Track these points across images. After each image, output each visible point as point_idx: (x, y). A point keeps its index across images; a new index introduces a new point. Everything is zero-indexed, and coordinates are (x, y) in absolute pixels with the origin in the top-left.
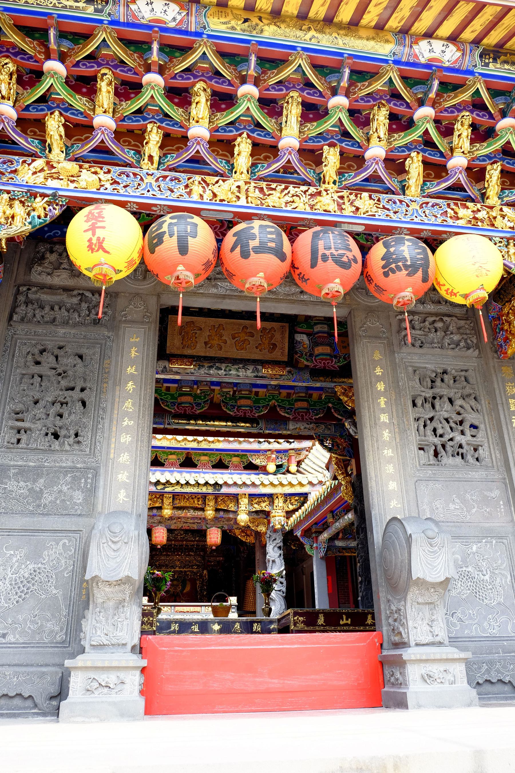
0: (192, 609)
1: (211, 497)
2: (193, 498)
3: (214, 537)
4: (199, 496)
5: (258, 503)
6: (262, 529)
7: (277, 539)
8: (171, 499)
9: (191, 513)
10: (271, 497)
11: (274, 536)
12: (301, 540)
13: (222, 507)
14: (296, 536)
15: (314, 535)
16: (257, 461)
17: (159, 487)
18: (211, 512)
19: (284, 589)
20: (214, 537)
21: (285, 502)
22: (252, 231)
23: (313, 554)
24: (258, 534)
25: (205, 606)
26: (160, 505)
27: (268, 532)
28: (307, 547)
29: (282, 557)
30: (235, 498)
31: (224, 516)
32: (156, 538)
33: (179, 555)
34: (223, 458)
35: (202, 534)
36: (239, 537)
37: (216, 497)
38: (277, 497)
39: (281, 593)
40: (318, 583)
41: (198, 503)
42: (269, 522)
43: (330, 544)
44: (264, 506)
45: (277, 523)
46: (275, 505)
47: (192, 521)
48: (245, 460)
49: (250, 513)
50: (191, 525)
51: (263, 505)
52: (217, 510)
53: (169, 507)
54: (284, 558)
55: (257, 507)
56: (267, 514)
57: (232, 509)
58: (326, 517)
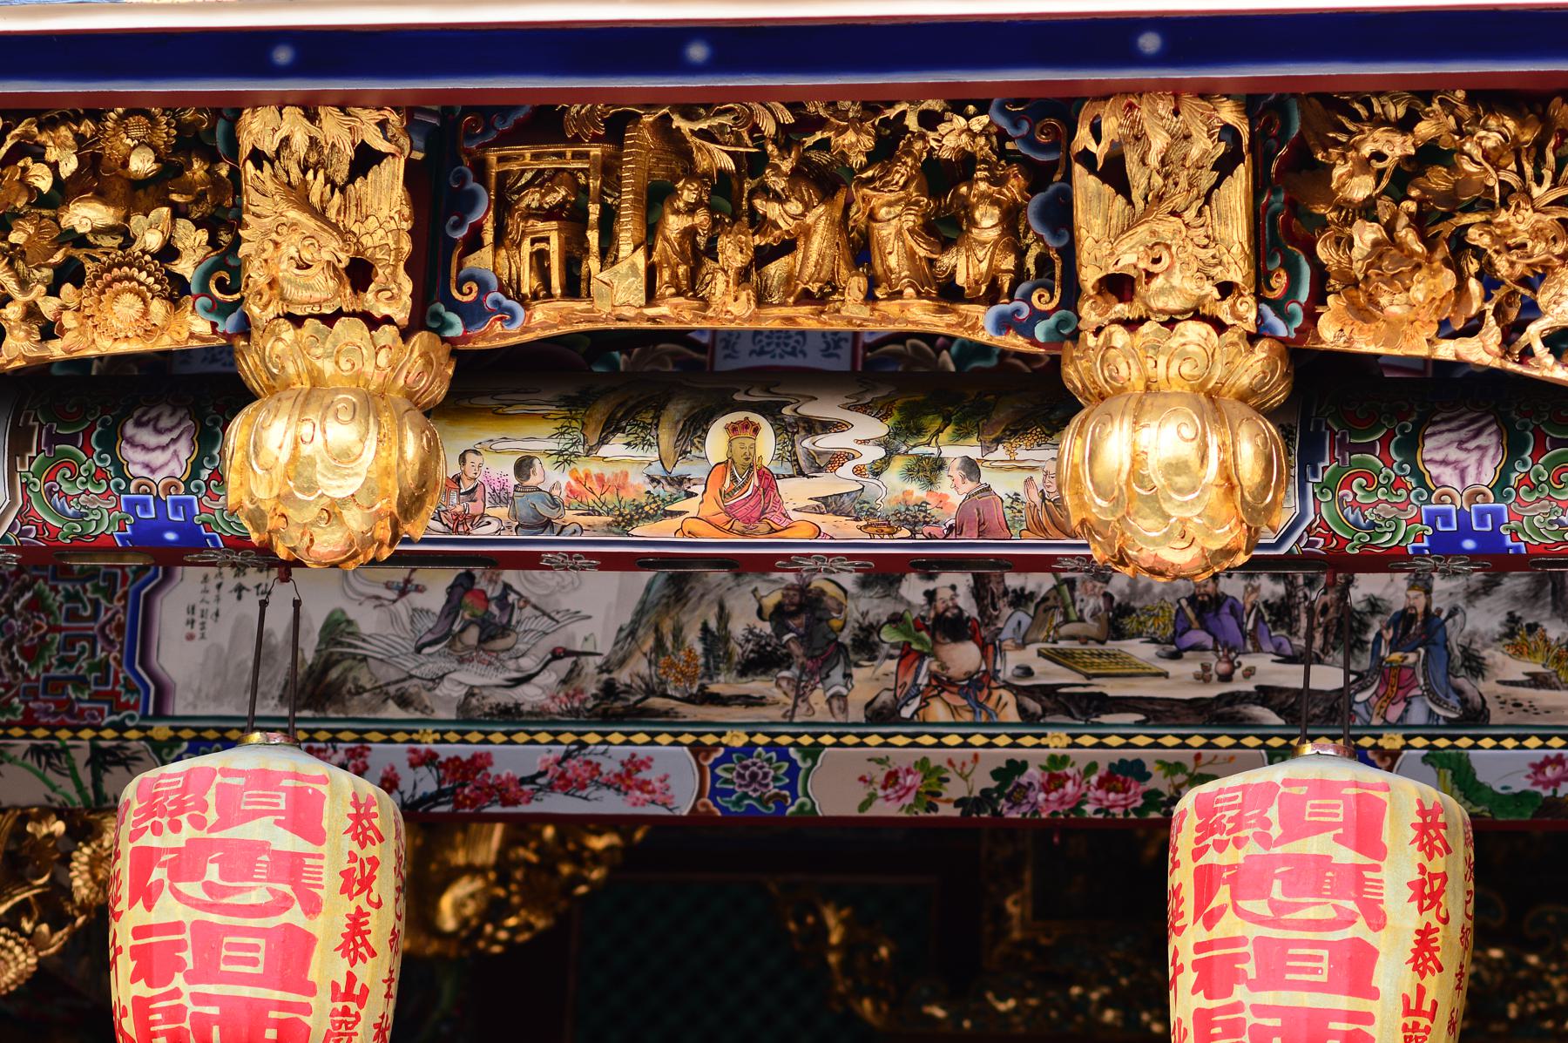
1: (1178, 130)
2: (825, 180)
4: (952, 137)
9: (848, 482)
13: (1405, 321)
18: (1166, 439)
22: (1140, 585)
26: (194, 326)
32: (150, 965)
47: (1182, 681)
52: (1331, 405)
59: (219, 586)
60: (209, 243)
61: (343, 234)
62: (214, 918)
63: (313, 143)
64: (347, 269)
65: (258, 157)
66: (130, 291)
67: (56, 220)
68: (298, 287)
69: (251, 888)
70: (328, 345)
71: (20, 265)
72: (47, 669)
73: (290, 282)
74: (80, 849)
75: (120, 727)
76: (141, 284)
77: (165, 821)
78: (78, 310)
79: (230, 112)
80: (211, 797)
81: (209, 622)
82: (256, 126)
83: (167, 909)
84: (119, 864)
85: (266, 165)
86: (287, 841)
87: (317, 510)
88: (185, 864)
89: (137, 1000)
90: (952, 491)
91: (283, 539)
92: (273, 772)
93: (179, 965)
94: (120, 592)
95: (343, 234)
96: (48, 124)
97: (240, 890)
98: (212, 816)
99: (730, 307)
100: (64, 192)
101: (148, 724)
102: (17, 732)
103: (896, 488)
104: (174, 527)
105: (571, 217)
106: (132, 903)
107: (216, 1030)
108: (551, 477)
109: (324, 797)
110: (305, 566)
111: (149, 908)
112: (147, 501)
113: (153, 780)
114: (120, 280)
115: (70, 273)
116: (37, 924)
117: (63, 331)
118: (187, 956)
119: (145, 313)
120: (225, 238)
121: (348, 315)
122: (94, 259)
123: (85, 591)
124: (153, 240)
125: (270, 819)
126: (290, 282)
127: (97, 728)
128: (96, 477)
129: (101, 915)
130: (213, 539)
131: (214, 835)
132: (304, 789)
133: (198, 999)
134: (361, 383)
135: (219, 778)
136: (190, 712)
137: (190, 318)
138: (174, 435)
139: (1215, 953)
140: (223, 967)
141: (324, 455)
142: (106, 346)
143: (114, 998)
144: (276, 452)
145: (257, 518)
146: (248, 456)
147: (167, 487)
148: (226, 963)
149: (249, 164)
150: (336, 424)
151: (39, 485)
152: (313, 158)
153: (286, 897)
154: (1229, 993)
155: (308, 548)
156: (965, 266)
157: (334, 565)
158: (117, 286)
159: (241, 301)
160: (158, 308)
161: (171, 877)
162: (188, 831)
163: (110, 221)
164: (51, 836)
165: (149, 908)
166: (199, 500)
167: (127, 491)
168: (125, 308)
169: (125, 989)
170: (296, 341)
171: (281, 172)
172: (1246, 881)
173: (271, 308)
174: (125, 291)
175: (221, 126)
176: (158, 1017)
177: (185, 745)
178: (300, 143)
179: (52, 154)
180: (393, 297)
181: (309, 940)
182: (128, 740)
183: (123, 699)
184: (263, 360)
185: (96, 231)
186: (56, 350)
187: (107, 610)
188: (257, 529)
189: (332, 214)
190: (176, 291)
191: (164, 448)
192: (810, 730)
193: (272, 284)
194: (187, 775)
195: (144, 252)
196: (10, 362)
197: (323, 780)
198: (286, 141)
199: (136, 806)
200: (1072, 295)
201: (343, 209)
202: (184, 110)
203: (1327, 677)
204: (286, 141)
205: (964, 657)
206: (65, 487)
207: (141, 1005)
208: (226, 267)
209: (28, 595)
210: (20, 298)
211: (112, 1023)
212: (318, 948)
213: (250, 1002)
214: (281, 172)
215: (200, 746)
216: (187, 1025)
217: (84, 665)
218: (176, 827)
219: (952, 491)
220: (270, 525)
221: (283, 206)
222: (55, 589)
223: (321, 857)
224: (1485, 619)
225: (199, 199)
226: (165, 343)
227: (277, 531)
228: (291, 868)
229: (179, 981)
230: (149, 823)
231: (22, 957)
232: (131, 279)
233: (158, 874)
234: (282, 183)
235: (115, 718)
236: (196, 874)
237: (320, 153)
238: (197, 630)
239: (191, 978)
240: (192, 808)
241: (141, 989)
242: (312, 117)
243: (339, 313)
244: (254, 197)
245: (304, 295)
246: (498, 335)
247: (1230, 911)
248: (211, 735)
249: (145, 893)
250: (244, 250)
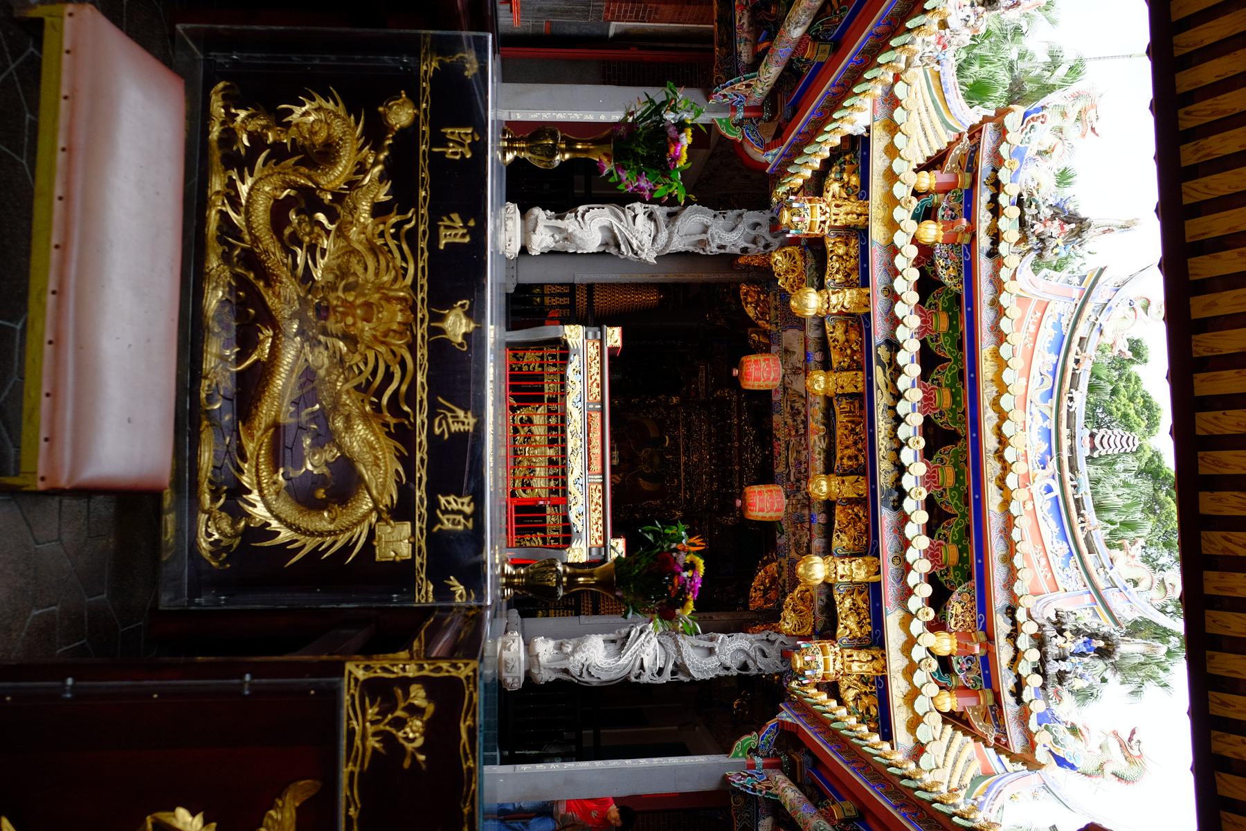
0: (597, 451)
1: (863, 488)
2: (855, 443)
3: (765, 503)
4: (862, 460)
5: (855, 609)
6: (789, 622)
7: (766, 661)
8: (854, 390)
9: (817, 442)
10: (875, 641)
11: (773, 652)
12: (770, 723)
13: (839, 516)
14: (780, 710)
15: (784, 758)
16: (959, 607)
17: (883, 352)
19: (645, 679)
20: (765, 503)
21: (863, 679)
23: (736, 756)
24: (771, 617)
25: (603, 484)
26: (835, 365)
27: (781, 638)
28: (750, 740)
29: (723, 673)
30: (868, 548)
31: (815, 527)
33: (710, 460)
34: (953, 521)
35: (766, 476)
36: (762, 573)
37: (868, 503)
38: (874, 658)
39: (636, 671)
40: (661, 768)
41: (843, 456)
42: (807, 638)
43: (763, 804)
44: (848, 625)
45: (807, 658)
46: (855, 653)
47: (791, 460)
48: (951, 577)
49: (828, 586)
50: (783, 458)
51: (852, 622)
52: (829, 506)
53: (832, 387)
54: (718, 676)
55: (844, 605)
56: (827, 631)
57: (836, 543)
58: (842, 799)
79: (861, 370)
88: (768, 366)
90: (817, 456)
99: (839, 432)
103: (817, 449)
105: (850, 412)
108: (817, 407)
141: (820, 383)
156: (845, 461)
172: (771, 496)
180: (839, 391)
200: (842, 475)
203: (792, 479)
205: (793, 433)
208: (843, 370)
219: (817, 456)
224: (800, 497)
246: (835, 403)
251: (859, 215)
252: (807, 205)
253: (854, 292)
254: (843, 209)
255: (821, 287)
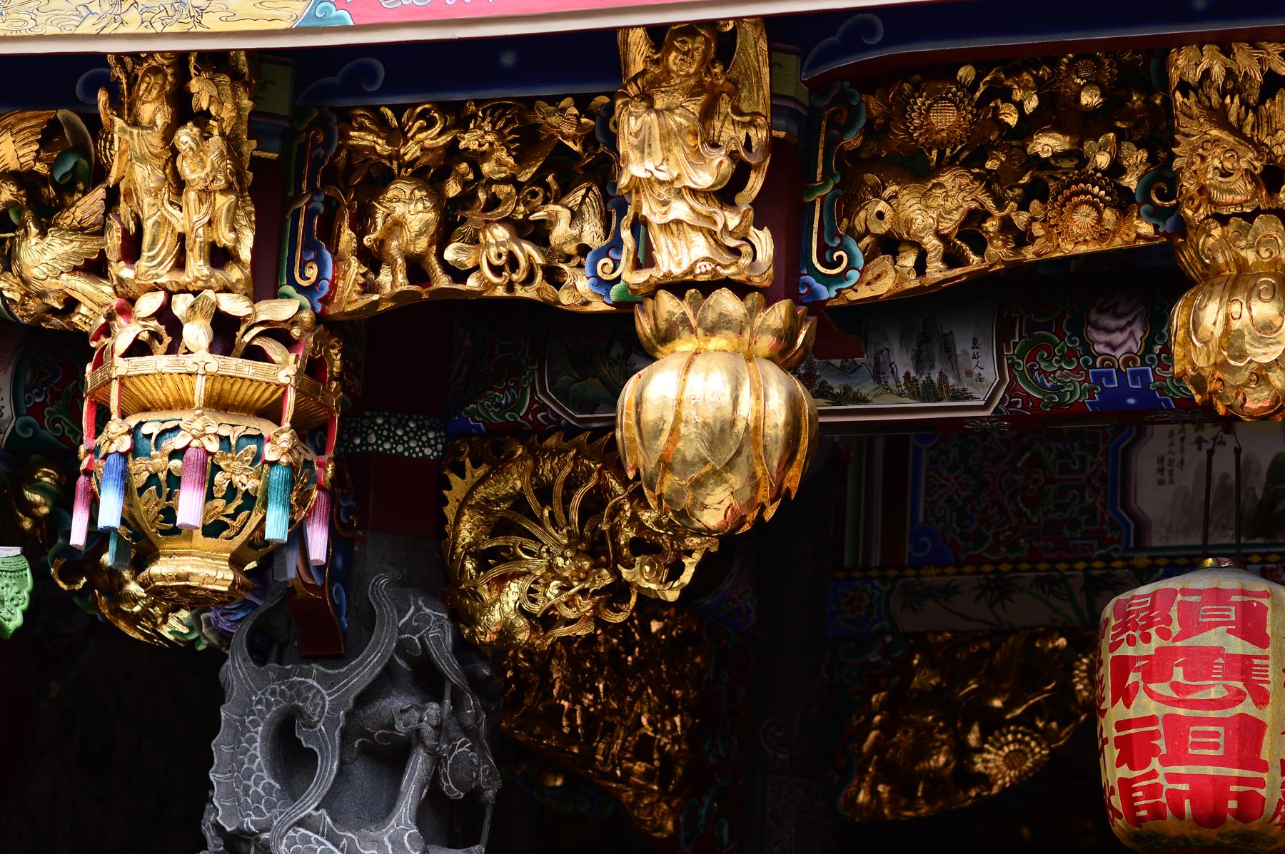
32: (1133, 752)
59: (1182, 440)
60: (1148, 160)
61: (1258, 146)
62: (1181, 711)
63: (1230, 74)
64: (1261, 174)
65: (1184, 87)
66: (1087, 202)
67: (1024, 148)
68: (1222, 191)
69: (1210, 686)
70: (1250, 238)
71: (997, 187)
72: (1045, 514)
73: (1215, 188)
74: (1080, 660)
75: (1108, 559)
76: (1094, 196)
77: (1137, 634)
78: (1044, 221)
79: (1160, 51)
80: (1174, 613)
81: (1176, 470)
82: (1181, 62)
83: (1144, 706)
84: (1102, 671)
85: (1192, 94)
86: (1237, 646)
87: (1247, 374)
88: (1156, 668)
89: (1122, 781)
91: (1220, 398)
92: (1224, 590)
93: (1154, 751)
94: (1102, 449)
95: (1258, 146)
96: (1014, 72)
97: (1201, 688)
98: (1175, 628)
100: (1030, 125)
101: (1130, 555)
102: (1024, 566)
104: (1134, 393)
106: (1114, 702)
107: (1187, 802)
109: (1267, 609)
110: (1241, 420)
111: (1128, 705)
112: (1111, 373)
113: (1128, 601)
114: (1077, 194)
115: (1036, 191)
116: (1048, 722)
117: (1033, 239)
118: (1161, 743)
119: (1100, 220)
120: (1162, 155)
121: (1265, 212)
122: (1056, 179)
123: (1074, 449)
124: (1103, 160)
125: (1223, 629)
126: (1215, 188)
127: (1089, 560)
128: (1068, 356)
129: (1094, 711)
130: (1166, 401)
131: (1179, 644)
132: (1251, 603)
133: (1171, 778)
134: (1279, 267)
135: (1179, 597)
136: (1163, 543)
137: (1136, 222)
138: (1130, 319)
139: (1132, 731)
140: (1190, 751)
142: (1068, 248)
143: (1104, 781)
144: (1212, 328)
145: (1199, 382)
146: (1188, 333)
147: (1126, 362)
148: (1193, 748)
149: (1178, 94)
150: (1259, 303)
151: (1023, 365)
152: (1230, 86)
153: (1239, 692)
154: (1148, 763)
155: (1242, 405)
157: (1265, 418)
158: (1076, 199)
159: (1178, 205)
160: (1109, 215)
161: (1143, 679)
162: (1156, 642)
163: (1067, 147)
164: (1056, 649)
165: (1128, 705)
166: (1153, 370)
167: (1094, 366)
168: (1083, 219)
169: (1113, 772)
170: (1223, 236)
171: (1204, 98)
173: (1201, 211)
174: (1082, 203)
175: (1154, 64)
176: (1140, 794)
177: (1161, 571)
178: (1218, 71)
179: (1018, 95)
181: (1259, 726)
182: (1115, 569)
183: (1109, 536)
184: (1197, 252)
185: (1056, 155)
186: (1029, 254)
187: (1092, 463)
188: (1199, 392)
189: (1247, 130)
190: (1123, 202)
191: (1121, 329)
192: (1182, 553)
193: (1202, 190)
194: (1153, 595)
195: (1096, 170)
196: (991, 266)
197: (1265, 595)
198: (1207, 73)
199: (1113, 622)
201: (1256, 126)
202: (1123, 52)
204: (1207, 73)
206: (1043, 365)
207: (1126, 784)
208: (1163, 177)
209: (1027, 455)
210: (997, 214)
211: (1104, 800)
212: (1268, 731)
213: (1214, 779)
214: (1204, 98)
215: (1173, 570)
216: (1163, 800)
217: (1076, 509)
218: (1147, 638)
220: (1210, 388)
221: (1207, 127)
222: (1049, 449)
223: (1266, 657)
225: (1139, 125)
226: (1117, 243)
227: (1215, 392)
228: (1243, 667)
229: (1155, 764)
230: (1124, 636)
231: (1037, 750)
232: (1086, 193)
233: (1133, 677)
234: (1205, 108)
235: (1103, 551)
236: (1165, 677)
237: (1236, 81)
238: (1166, 477)
239: (1165, 762)
240: (1159, 622)
241: (1125, 772)
242: (1227, 52)
243: (1257, 212)
244: (1183, 119)
245: (1228, 198)
247: (1142, 693)
248: (1182, 561)
249: (1125, 694)
250: (1177, 163)
251: (183, 110)
252: (117, 436)
253: (632, 123)
254: (151, 207)
255: (617, 344)
